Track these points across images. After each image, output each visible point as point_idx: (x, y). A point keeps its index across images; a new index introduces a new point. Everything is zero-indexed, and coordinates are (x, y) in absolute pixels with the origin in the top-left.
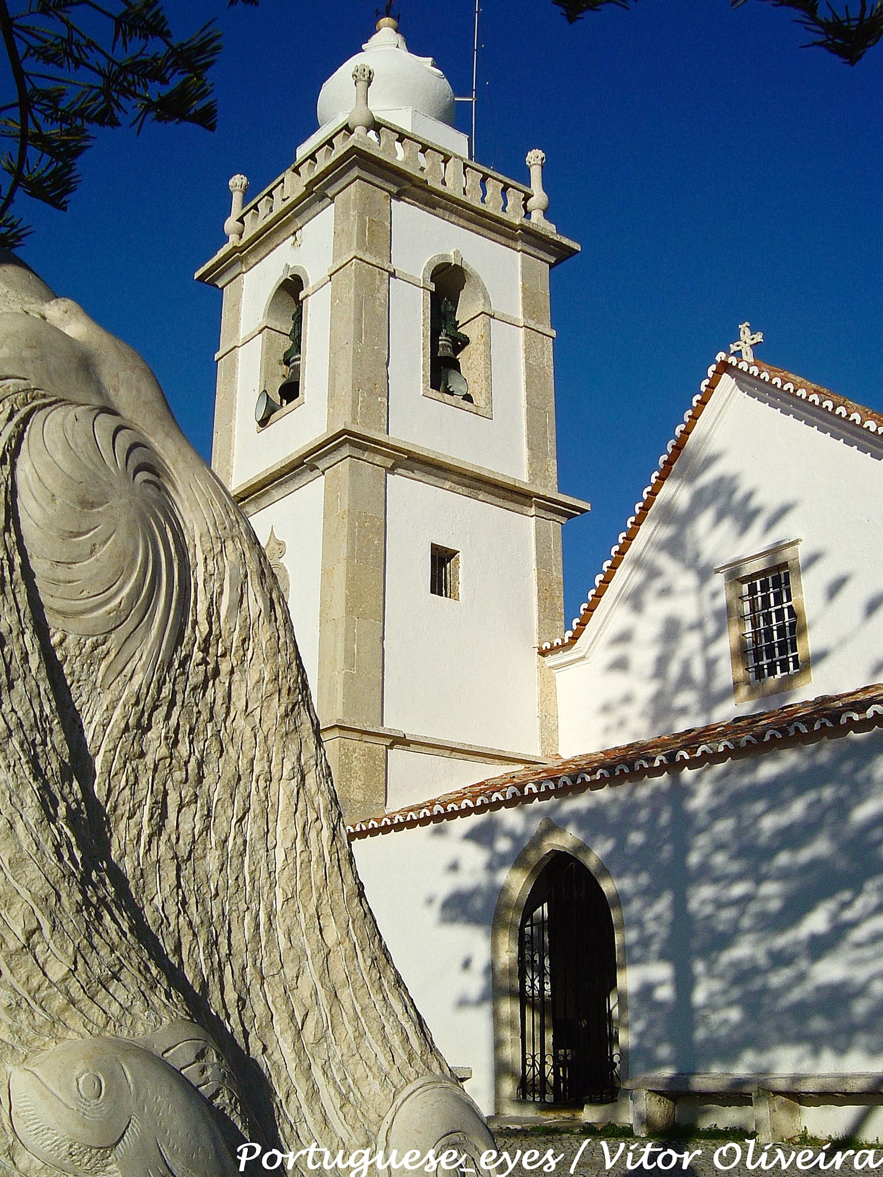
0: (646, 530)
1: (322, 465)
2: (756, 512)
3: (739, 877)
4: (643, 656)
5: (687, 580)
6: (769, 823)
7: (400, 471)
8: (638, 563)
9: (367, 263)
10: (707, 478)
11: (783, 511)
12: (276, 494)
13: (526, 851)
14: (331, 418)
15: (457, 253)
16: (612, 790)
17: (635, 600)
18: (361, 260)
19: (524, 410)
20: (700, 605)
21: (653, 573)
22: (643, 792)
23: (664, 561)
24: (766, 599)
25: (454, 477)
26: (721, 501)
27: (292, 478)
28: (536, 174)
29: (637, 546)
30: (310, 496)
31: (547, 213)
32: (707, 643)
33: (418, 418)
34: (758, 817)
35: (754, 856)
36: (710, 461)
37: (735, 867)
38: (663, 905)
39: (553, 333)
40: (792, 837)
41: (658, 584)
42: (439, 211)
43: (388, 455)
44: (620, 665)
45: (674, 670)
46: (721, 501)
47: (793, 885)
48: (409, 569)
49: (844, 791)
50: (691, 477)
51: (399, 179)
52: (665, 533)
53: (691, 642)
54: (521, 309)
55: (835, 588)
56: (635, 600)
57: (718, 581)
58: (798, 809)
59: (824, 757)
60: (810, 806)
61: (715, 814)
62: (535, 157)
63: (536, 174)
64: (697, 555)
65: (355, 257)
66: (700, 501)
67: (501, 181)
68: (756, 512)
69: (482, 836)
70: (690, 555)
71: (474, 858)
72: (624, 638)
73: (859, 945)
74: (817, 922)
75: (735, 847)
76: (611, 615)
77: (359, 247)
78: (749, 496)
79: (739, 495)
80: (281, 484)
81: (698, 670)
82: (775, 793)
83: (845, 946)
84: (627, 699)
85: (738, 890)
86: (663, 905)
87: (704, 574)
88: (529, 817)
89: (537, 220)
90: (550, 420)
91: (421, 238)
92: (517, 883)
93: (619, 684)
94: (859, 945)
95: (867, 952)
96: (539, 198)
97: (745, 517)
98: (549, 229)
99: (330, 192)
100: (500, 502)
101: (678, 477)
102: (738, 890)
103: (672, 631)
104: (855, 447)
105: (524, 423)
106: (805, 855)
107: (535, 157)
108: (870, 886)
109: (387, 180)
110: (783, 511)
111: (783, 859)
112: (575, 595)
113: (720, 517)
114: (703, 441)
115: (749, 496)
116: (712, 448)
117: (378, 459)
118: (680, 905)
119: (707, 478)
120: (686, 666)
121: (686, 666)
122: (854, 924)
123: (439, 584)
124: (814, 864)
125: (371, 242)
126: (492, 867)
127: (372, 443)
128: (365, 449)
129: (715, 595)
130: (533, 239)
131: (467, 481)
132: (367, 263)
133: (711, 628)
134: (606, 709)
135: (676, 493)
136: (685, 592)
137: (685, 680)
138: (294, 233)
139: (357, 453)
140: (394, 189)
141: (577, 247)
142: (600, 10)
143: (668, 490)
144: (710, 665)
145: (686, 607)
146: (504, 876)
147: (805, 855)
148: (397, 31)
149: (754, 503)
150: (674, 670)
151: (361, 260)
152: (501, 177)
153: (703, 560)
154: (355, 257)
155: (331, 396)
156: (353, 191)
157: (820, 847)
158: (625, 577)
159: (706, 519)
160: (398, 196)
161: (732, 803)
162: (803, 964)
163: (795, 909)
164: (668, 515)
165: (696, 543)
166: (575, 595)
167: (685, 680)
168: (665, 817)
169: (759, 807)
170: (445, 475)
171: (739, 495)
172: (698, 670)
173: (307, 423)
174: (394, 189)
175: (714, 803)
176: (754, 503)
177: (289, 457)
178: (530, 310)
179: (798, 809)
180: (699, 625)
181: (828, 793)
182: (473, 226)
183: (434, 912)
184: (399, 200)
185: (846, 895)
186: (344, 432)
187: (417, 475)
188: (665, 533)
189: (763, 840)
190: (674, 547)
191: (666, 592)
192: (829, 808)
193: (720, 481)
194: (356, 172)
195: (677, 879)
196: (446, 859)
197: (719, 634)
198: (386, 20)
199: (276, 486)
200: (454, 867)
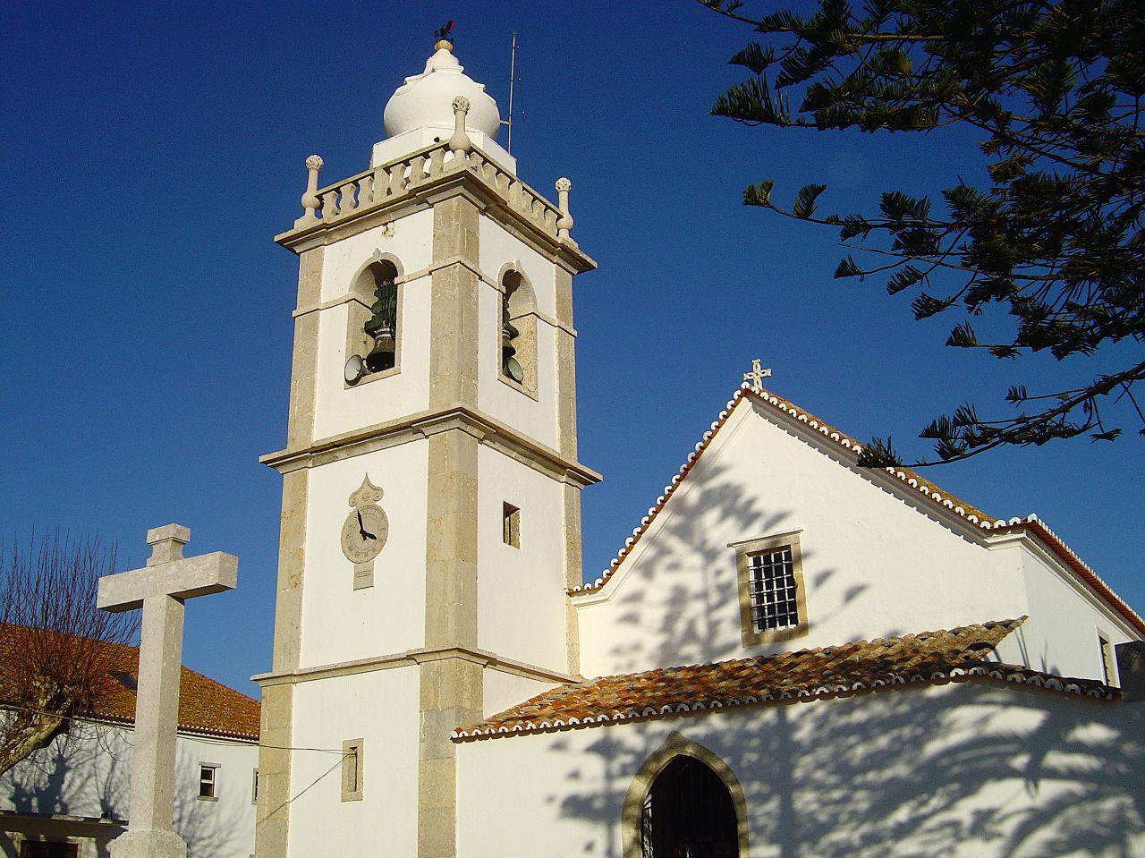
0: (662, 517)
1: (427, 431)
2: (757, 515)
3: (836, 787)
4: (653, 613)
5: (696, 560)
6: (860, 751)
7: (486, 441)
8: (652, 541)
9: (466, 267)
10: (715, 483)
11: (780, 517)
12: (371, 447)
13: (647, 762)
14: (434, 394)
15: (518, 262)
16: (728, 718)
17: (647, 569)
18: (463, 264)
19: (557, 395)
20: (705, 580)
21: (664, 551)
22: (753, 726)
23: (674, 543)
24: (769, 585)
25: (521, 450)
26: (727, 503)
27: (392, 437)
28: (564, 197)
29: (654, 527)
30: (416, 452)
31: (571, 232)
32: (710, 610)
33: (496, 402)
34: (851, 747)
35: (846, 772)
36: (718, 471)
37: (833, 779)
38: (773, 805)
39: (575, 333)
40: (878, 761)
41: (667, 560)
42: (508, 226)
43: (482, 430)
44: (631, 619)
45: (680, 627)
46: (727, 503)
47: (880, 794)
48: (490, 522)
49: (919, 731)
50: (701, 481)
51: (488, 199)
52: (675, 521)
53: (695, 609)
54: (555, 312)
55: (821, 579)
56: (647, 569)
57: (724, 562)
58: (883, 742)
59: (904, 708)
60: (894, 740)
61: (816, 743)
62: (563, 184)
63: (564, 197)
64: (704, 542)
65: (459, 262)
66: (708, 500)
67: (544, 204)
68: (757, 515)
69: (605, 749)
70: (697, 540)
71: (594, 767)
72: (635, 598)
73: (930, 831)
74: (902, 814)
75: (832, 766)
76: (625, 579)
77: (462, 252)
78: (751, 502)
79: (742, 500)
80: (381, 439)
81: (702, 629)
82: (864, 731)
83: (920, 830)
84: (637, 647)
85: (837, 795)
86: (773, 805)
87: (710, 555)
88: (650, 738)
89: (564, 234)
90: (573, 405)
91: (500, 248)
92: (639, 787)
93: (628, 634)
94: (930, 831)
95: (936, 836)
96: (567, 220)
97: (747, 516)
98: (574, 246)
99: (431, 200)
100: (544, 470)
101: (692, 480)
102: (837, 795)
103: (678, 598)
104: (938, 522)
105: (557, 406)
106: (888, 774)
107: (563, 184)
108: (940, 791)
109: (481, 199)
110: (780, 517)
111: (871, 776)
112: (596, 556)
113: (725, 515)
114: (714, 455)
115: (751, 502)
116: (722, 460)
117: (475, 432)
118: (787, 804)
119: (715, 483)
120: (691, 626)
121: (691, 626)
122: (926, 817)
123: (510, 536)
124: (894, 781)
125: (468, 249)
126: (609, 777)
127: (1115, 620)
128: (468, 423)
129: (719, 573)
130: (566, 255)
131: (528, 453)
132: (466, 267)
133: (714, 598)
134: (617, 651)
135: (689, 492)
136: (692, 569)
137: (690, 635)
138: (386, 224)
139: (463, 426)
140: (483, 206)
141: (595, 264)
142: (850, 259)
143: (683, 488)
144: (713, 627)
145: (693, 581)
146: (622, 784)
147: (888, 774)
148: (451, 53)
149: (757, 507)
150: (680, 627)
151: (463, 264)
152: (545, 200)
153: (710, 545)
154: (459, 262)
155: (434, 372)
156: (455, 203)
157: (901, 770)
158: (641, 551)
159: (711, 516)
160: (483, 212)
161: (830, 734)
162: (889, 843)
163: (882, 808)
164: (680, 508)
165: (703, 532)
166: (596, 556)
167: (690, 635)
168: (774, 745)
169: (852, 740)
170: (513, 446)
171: (742, 500)
172: (702, 629)
173: (406, 392)
174: (483, 206)
175: (816, 735)
176: (757, 507)
177: (397, 420)
178: (561, 314)
179: (883, 742)
180: (704, 595)
181: (907, 732)
182: (529, 241)
183: (555, 809)
184: (483, 214)
185: (925, 796)
186: (461, 409)
187: (497, 446)
188: (675, 521)
189: (855, 762)
190: (684, 532)
191: (675, 567)
192: (908, 742)
193: (727, 486)
194: (460, 189)
195: (785, 787)
196: (569, 768)
197: (722, 603)
198: (444, 43)
199: (373, 441)
200: (575, 775)
